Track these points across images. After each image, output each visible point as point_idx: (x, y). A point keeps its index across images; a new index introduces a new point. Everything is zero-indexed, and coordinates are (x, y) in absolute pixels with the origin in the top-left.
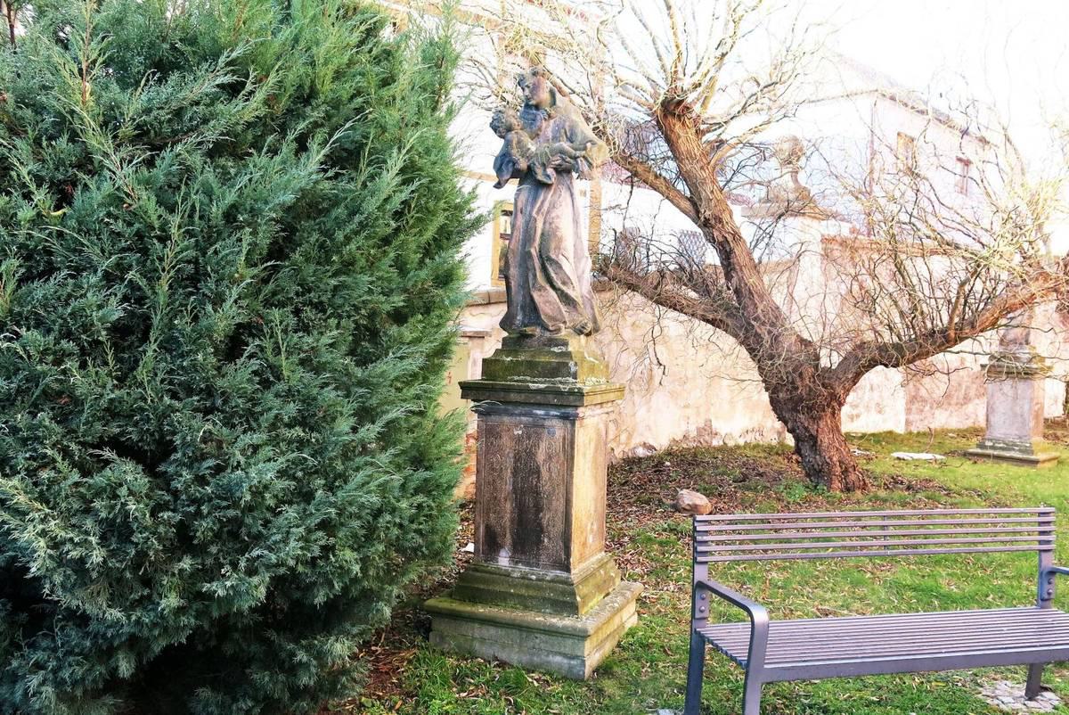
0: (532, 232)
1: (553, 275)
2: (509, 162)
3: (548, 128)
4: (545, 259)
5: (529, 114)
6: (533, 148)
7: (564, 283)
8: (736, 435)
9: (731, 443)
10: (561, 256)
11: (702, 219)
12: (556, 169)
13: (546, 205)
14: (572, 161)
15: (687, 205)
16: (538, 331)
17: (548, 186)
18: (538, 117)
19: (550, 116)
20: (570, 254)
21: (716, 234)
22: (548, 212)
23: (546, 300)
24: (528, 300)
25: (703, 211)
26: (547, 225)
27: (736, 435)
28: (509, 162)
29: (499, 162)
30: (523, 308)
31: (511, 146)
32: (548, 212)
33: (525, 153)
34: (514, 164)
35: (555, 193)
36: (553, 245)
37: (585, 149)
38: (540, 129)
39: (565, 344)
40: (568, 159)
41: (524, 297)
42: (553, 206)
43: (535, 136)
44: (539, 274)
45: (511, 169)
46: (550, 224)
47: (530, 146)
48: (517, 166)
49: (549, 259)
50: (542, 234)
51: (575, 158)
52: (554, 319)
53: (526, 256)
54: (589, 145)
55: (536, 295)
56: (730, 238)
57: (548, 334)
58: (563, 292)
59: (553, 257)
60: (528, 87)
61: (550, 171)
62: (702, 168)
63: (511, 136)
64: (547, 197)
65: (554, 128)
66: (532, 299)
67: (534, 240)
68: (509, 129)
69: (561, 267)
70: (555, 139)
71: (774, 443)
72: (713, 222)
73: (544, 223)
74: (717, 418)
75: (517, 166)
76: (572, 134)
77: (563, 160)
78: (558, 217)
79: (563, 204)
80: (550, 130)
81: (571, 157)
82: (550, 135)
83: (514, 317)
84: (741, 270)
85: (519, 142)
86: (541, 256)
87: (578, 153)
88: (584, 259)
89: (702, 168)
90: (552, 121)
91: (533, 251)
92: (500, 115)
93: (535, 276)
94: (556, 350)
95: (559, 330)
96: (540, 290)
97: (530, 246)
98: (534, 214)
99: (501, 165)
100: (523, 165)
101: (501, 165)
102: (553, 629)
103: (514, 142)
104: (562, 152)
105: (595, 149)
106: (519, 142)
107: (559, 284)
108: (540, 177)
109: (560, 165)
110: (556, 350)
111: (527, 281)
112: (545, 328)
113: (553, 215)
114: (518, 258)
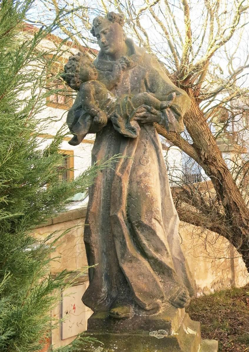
0: (117, 194)
1: (145, 242)
2: (86, 114)
3: (127, 79)
4: (135, 225)
5: (105, 64)
6: (113, 99)
7: (157, 250)
8: (209, 287)
9: (207, 293)
10: (154, 221)
11: (203, 159)
12: (139, 122)
13: (131, 162)
14: (158, 112)
15: (191, 150)
16: (131, 311)
17: (129, 140)
18: (117, 67)
19: (129, 65)
20: (160, 216)
21: (213, 168)
22: (134, 170)
23: (138, 272)
24: (115, 270)
25: (203, 153)
26: (135, 185)
27: (209, 287)
28: (86, 114)
29: (74, 117)
30: (108, 277)
31: (89, 97)
32: (134, 170)
33: (104, 104)
34: (93, 117)
35: (139, 147)
36: (144, 208)
37: (171, 98)
38: (118, 79)
39: (167, 327)
40: (154, 110)
41: (109, 265)
42: (139, 162)
43: (113, 87)
44: (129, 242)
45: (89, 123)
46: (138, 183)
47: (109, 97)
48: (96, 119)
49: (141, 225)
50: (129, 195)
51: (162, 109)
52: (151, 296)
53: (110, 221)
54: (174, 94)
55: (126, 268)
56: (222, 171)
57: (143, 314)
58: (156, 260)
59: (146, 222)
60: (104, 33)
61: (133, 124)
62: (202, 124)
63: (88, 85)
64: (129, 154)
65: (132, 78)
66: (121, 271)
67: (121, 204)
68: (85, 79)
69: (154, 233)
70: (135, 89)
71: (229, 287)
72: (210, 161)
73: (131, 182)
74: (198, 279)
75: (96, 119)
76: (152, 85)
77: (148, 111)
78: (146, 175)
79: (150, 159)
80: (128, 80)
81: (157, 108)
82: (129, 86)
83: (99, 290)
84: (230, 192)
85: (97, 93)
86: (129, 221)
87: (165, 104)
88: (172, 219)
89: (202, 124)
90: (130, 72)
91: (119, 215)
92: (74, 63)
93: (124, 245)
94: (155, 334)
95: (157, 308)
96: (131, 261)
97: (116, 210)
98: (118, 172)
99: (77, 119)
100: (103, 117)
101: (77, 119)
102: (48, 227)
103: (92, 92)
104: (147, 102)
105: (180, 99)
106: (97, 93)
107: (151, 251)
108: (123, 131)
109: (144, 117)
110: (155, 334)
111: (113, 247)
112: (140, 307)
113: (141, 172)
114: (100, 222)
